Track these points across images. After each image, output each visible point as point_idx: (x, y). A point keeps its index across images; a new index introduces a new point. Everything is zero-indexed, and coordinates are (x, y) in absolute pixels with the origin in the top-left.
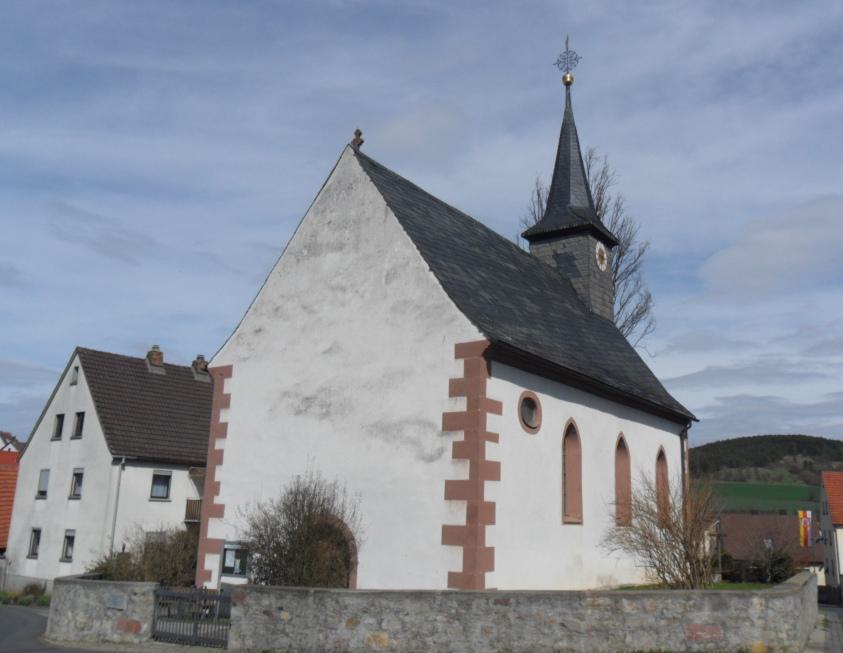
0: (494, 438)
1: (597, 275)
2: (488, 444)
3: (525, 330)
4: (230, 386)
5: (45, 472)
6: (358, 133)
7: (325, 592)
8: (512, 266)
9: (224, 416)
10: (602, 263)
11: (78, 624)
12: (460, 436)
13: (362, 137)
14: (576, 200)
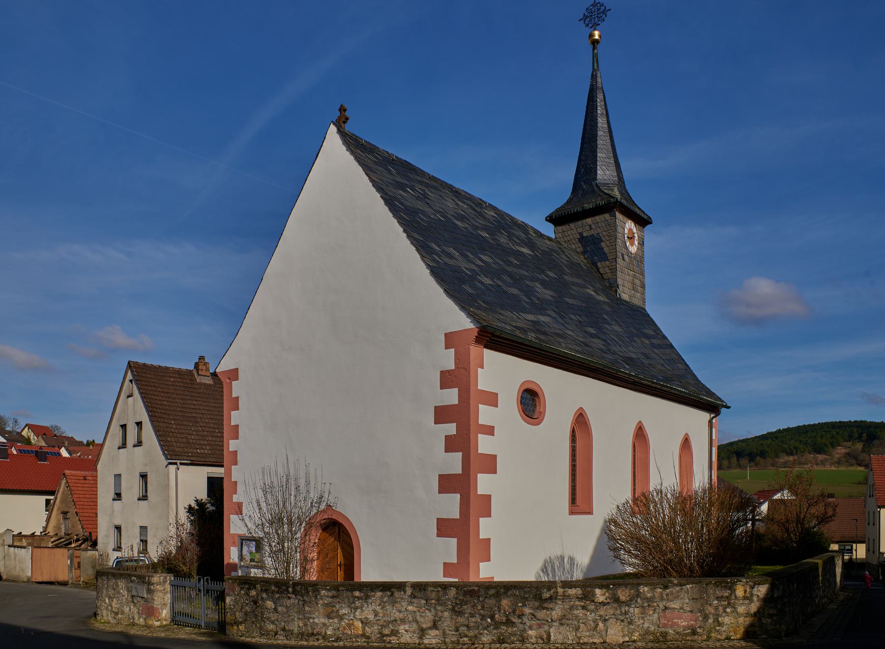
0: (489, 430)
1: (626, 257)
2: (481, 437)
3: (530, 317)
4: (237, 389)
5: (118, 477)
6: (342, 109)
7: (580, 565)
8: (525, 250)
9: (235, 417)
10: (632, 244)
11: (114, 609)
12: (451, 429)
13: (347, 114)
14: (604, 173)
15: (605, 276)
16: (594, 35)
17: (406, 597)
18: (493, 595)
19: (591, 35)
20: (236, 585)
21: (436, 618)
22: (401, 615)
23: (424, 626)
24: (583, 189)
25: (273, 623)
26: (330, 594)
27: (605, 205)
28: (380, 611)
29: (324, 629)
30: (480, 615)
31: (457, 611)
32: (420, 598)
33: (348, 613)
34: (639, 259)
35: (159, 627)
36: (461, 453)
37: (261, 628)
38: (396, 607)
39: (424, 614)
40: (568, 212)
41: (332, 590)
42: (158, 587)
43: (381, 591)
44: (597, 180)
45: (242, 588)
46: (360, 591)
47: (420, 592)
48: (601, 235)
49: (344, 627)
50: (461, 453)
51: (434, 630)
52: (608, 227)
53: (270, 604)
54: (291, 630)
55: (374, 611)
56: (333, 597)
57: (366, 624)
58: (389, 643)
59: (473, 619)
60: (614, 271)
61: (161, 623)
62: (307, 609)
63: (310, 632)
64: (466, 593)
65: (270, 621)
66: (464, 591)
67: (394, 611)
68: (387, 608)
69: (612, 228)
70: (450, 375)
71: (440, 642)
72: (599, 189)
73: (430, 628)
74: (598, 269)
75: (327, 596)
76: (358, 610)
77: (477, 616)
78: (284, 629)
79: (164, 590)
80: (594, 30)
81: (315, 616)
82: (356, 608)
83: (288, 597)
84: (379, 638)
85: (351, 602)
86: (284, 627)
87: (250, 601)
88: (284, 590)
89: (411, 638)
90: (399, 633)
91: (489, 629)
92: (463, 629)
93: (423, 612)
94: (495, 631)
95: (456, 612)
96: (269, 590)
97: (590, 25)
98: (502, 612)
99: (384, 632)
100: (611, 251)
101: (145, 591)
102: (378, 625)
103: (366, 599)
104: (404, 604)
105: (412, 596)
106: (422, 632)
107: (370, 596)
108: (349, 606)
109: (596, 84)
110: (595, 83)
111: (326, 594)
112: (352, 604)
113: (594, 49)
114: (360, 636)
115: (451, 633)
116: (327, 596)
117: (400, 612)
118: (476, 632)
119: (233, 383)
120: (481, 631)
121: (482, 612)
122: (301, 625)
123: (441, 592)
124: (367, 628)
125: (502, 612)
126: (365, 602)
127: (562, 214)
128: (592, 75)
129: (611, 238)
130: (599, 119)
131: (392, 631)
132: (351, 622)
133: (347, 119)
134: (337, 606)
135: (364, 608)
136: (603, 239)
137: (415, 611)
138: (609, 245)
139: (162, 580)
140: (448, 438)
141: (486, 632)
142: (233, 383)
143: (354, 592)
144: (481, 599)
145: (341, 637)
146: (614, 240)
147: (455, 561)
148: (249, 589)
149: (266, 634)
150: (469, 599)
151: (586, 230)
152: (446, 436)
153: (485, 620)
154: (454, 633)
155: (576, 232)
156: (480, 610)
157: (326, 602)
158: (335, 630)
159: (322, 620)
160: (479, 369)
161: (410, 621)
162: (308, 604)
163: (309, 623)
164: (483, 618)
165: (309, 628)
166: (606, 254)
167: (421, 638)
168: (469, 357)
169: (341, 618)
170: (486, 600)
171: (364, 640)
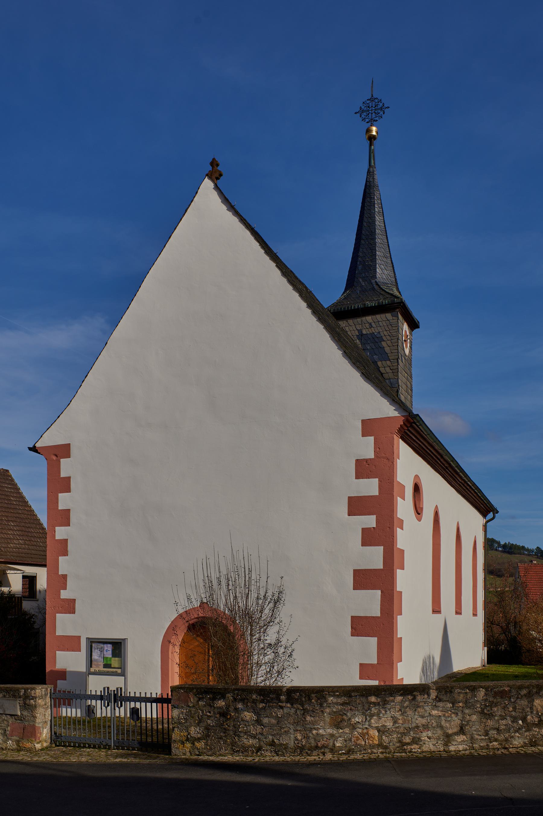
12: (370, 521)
15: (386, 376)
16: (371, 131)
17: (430, 700)
18: (525, 695)
19: (369, 131)
20: (191, 695)
21: (463, 723)
22: (424, 721)
23: (450, 732)
24: (362, 286)
25: (254, 737)
26: (340, 701)
27: (388, 304)
28: (400, 718)
29: (331, 741)
30: (511, 716)
31: (486, 714)
32: (445, 701)
33: (362, 721)
34: (409, 361)
35: (41, 750)
36: (382, 547)
37: (233, 744)
38: (418, 713)
39: (450, 719)
40: (348, 307)
41: (342, 696)
42: (40, 701)
43: (401, 695)
44: (376, 278)
45: (200, 699)
46: (377, 696)
47: (446, 694)
48: (382, 335)
49: (357, 737)
50: (382, 547)
51: (461, 735)
52: (390, 327)
53: (248, 715)
54: (284, 745)
55: (393, 717)
56: (343, 704)
57: (383, 732)
58: (410, 752)
59: (504, 722)
60: (396, 372)
61: (42, 745)
62: (308, 718)
63: (313, 745)
64: (496, 695)
65: (248, 735)
66: (495, 692)
67: (416, 717)
68: (408, 713)
69: (394, 328)
70: (369, 465)
71: (468, 748)
72: (380, 287)
73: (456, 734)
74: (378, 368)
75: (337, 704)
76: (375, 717)
77: (508, 718)
78: (272, 744)
79: (45, 704)
80: (371, 125)
81: (319, 727)
82: (372, 716)
83: (280, 706)
84: (398, 747)
85: (366, 708)
86: (273, 741)
87: (214, 713)
88: (272, 699)
89: (434, 745)
90: (422, 740)
91: (521, 732)
92: (492, 733)
93: (448, 717)
94: (527, 733)
95: (486, 714)
96: (248, 699)
97: (367, 120)
98: (535, 712)
99: (404, 741)
100: (392, 351)
101: (18, 707)
102: (398, 733)
103: (385, 704)
104: (427, 708)
105: (437, 699)
106: (448, 738)
107: (388, 701)
108: (363, 714)
109: (374, 181)
110: (372, 180)
111: (335, 701)
112: (367, 711)
113: (371, 145)
114: (376, 747)
115: (480, 737)
116: (337, 704)
117: (423, 717)
118: (507, 735)
119: (62, 461)
120: (513, 734)
121: (513, 713)
122: (299, 738)
123: (469, 694)
124: (384, 737)
125: (535, 712)
126: (382, 708)
127: (341, 308)
128: (369, 172)
129: (392, 338)
130: (376, 217)
131: (414, 738)
132: (365, 731)
133: (221, 175)
134: (348, 714)
135: (381, 715)
136: (384, 338)
137: (440, 716)
138: (390, 344)
139: (43, 693)
140: (365, 531)
141: (517, 734)
142: (62, 461)
143: (369, 698)
144: (512, 700)
145: (353, 749)
146: (396, 340)
147: (375, 662)
148: (214, 699)
149: (245, 750)
150: (499, 700)
151: (365, 328)
152: (363, 529)
153: (517, 722)
154: (483, 737)
155: (355, 329)
156: (511, 711)
157: (334, 710)
158: (346, 741)
159: (330, 731)
160: (398, 460)
161: (434, 727)
162: (311, 713)
163: (311, 735)
164: (515, 720)
165: (312, 741)
166: (387, 354)
167: (446, 744)
168: (393, 447)
169: (354, 727)
170: (518, 701)
171: (380, 750)
